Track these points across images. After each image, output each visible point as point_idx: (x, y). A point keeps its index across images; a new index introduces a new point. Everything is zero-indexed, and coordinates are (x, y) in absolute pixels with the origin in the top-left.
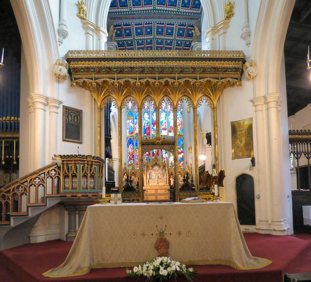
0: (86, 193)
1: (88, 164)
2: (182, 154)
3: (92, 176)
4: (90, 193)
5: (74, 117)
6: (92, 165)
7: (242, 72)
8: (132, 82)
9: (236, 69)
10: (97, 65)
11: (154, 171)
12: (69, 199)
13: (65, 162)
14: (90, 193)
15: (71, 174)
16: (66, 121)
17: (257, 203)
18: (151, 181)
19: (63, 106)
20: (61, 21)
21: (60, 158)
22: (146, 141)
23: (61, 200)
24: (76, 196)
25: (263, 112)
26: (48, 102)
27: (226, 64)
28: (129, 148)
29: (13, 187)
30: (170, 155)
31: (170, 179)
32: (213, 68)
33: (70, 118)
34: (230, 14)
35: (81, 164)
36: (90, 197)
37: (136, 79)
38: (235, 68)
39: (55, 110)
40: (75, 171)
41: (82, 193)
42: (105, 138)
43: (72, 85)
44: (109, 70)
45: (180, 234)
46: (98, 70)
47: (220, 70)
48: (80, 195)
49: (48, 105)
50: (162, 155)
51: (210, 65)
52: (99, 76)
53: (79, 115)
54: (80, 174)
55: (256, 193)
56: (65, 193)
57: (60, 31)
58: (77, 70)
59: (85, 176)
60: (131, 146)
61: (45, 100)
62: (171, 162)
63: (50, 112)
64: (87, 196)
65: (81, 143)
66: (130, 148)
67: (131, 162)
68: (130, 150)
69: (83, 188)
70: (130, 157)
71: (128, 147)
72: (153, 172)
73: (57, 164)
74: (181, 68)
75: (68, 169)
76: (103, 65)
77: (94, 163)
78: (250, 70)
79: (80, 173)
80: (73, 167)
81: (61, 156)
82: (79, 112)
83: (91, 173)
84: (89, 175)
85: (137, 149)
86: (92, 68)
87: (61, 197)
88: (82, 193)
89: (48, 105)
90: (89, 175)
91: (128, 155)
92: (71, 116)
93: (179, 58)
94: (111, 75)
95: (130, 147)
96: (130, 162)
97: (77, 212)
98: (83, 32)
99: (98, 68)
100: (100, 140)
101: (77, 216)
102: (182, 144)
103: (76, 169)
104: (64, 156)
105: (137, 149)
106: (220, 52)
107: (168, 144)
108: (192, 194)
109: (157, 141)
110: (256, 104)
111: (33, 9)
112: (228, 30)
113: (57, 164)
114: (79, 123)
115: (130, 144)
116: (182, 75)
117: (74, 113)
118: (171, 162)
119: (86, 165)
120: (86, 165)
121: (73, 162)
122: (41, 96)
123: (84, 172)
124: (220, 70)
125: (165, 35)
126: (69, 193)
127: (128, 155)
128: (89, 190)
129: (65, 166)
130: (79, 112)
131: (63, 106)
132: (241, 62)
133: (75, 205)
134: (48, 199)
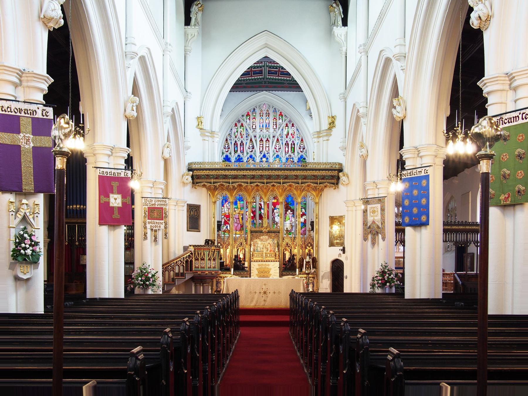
0: (211, 271)
1: (212, 251)
2: (304, 217)
3: (214, 260)
4: (213, 271)
5: (195, 211)
6: (215, 251)
7: (338, 178)
8: (244, 185)
9: (333, 177)
10: (216, 173)
11: (262, 240)
12: (199, 274)
13: (196, 250)
14: (213, 271)
15: (201, 258)
16: (189, 215)
17: (345, 280)
18: (256, 255)
19: (187, 204)
20: (129, 39)
21: (193, 247)
22: (239, 160)
23: (193, 275)
24: (197, 273)
25: (506, 105)
26: (22, 79)
27: (324, 173)
28: (224, 207)
29: (165, 266)
30: (285, 218)
31: (285, 253)
32: (313, 176)
33: (192, 213)
34: (332, 124)
35: (207, 251)
36: (213, 274)
37: (248, 183)
38: (332, 176)
39: (181, 208)
40: (203, 256)
41: (208, 271)
42: (218, 224)
43: (193, 187)
44: (225, 177)
45: (274, 293)
46: (216, 177)
47: (319, 177)
48: (207, 272)
49: (21, 85)
50: (274, 218)
51: (310, 173)
52: (217, 180)
53: (198, 209)
54: (206, 258)
55: (345, 274)
56: (196, 271)
57: (127, 53)
58: (199, 177)
59: (210, 259)
60: (227, 205)
61: (16, 77)
62: (287, 229)
63: (178, 210)
64: (211, 273)
65: (200, 231)
66: (226, 208)
67: (227, 228)
68: (226, 209)
69: (208, 268)
70: (225, 220)
71: (223, 206)
72: (260, 243)
73: (191, 251)
74: (286, 176)
75: (198, 255)
76: (221, 173)
77: (216, 250)
78: (343, 178)
79: (206, 258)
80: (202, 253)
81: (193, 246)
82: (198, 207)
83: (214, 257)
84: (212, 259)
85: (236, 209)
86: (211, 176)
87: (194, 273)
88: (208, 271)
89: (21, 85)
90: (212, 259)
91: (223, 217)
92: (193, 211)
93: (284, 169)
94: (226, 180)
95: (225, 205)
96: (225, 227)
97: (201, 284)
98: (201, 138)
99: (216, 175)
100: (214, 229)
101: (202, 288)
102: (305, 203)
103: (204, 255)
104: (195, 245)
105: (236, 209)
106: (319, 164)
107: (274, 232)
108: (294, 273)
109: (264, 230)
110: (348, 205)
111: (100, 38)
112: (331, 138)
113: (191, 251)
114: (198, 216)
115: (225, 202)
116: (286, 180)
117: (195, 208)
118: (287, 229)
119: (211, 253)
120: (211, 252)
121: (202, 250)
122: (106, 147)
123: (214, 257)
124: (319, 177)
125: (280, 75)
126: (199, 271)
127: (223, 217)
128: (212, 269)
129: (196, 252)
130: (198, 207)
131: (187, 204)
132: (336, 172)
133: (201, 279)
134: (176, 280)
